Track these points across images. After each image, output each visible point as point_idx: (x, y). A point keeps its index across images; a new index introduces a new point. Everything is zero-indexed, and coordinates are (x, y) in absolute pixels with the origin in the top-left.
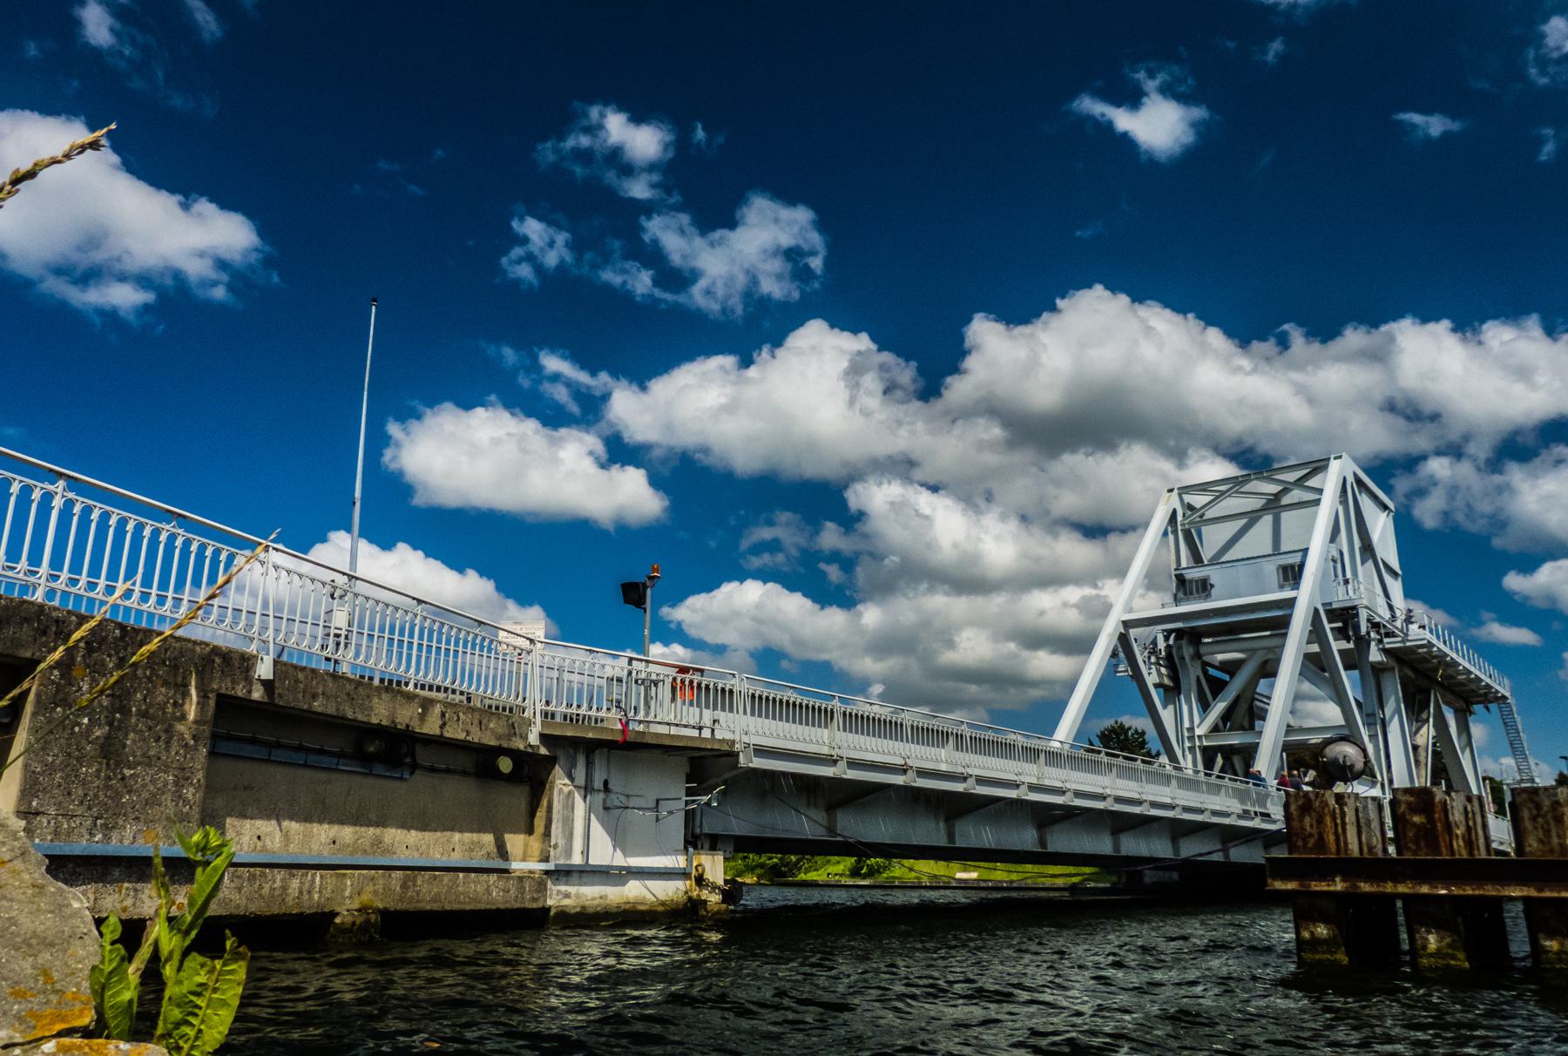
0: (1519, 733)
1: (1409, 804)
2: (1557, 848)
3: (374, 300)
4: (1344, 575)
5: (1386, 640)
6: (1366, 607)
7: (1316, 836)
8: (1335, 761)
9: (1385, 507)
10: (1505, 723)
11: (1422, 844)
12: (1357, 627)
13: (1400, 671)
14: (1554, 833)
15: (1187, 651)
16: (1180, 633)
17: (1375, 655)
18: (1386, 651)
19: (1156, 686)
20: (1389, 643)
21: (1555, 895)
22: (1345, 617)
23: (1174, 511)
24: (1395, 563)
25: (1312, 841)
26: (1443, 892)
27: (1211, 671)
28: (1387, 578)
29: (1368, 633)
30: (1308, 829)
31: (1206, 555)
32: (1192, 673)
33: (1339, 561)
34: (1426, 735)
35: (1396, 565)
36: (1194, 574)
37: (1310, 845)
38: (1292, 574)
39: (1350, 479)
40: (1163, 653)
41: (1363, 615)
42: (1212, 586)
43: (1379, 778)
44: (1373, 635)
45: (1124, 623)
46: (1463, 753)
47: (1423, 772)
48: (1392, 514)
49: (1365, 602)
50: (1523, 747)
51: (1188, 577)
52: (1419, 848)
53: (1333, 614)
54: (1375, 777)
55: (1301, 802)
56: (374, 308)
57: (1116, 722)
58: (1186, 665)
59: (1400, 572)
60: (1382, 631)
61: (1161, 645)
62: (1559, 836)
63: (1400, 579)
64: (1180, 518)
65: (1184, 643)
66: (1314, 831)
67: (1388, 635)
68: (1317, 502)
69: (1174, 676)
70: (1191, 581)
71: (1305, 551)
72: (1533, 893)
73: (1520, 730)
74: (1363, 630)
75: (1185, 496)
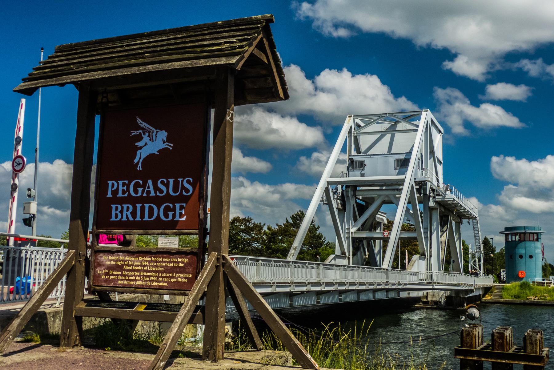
0: (478, 232)
1: (498, 336)
2: (534, 351)
3: (42, 49)
4: (422, 167)
5: (437, 197)
6: (430, 182)
7: (470, 343)
8: (471, 314)
9: (440, 132)
10: (474, 228)
11: (500, 348)
12: (425, 190)
13: (440, 209)
14: (534, 348)
15: (350, 193)
16: (347, 187)
17: (431, 204)
18: (436, 202)
19: (336, 208)
20: (438, 199)
21: (533, 364)
22: (421, 185)
23: (351, 127)
24: (441, 159)
25: (469, 344)
26: (504, 361)
27: (358, 201)
28: (438, 165)
29: (430, 193)
30: (468, 341)
31: (363, 148)
32: (351, 204)
33: (421, 159)
34: (444, 238)
35: (441, 159)
36: (358, 159)
37: (468, 345)
38: (403, 164)
39: (430, 122)
40: (340, 194)
41: (429, 185)
42: (365, 165)
43: (427, 256)
44: (431, 194)
45: (328, 182)
46: (457, 241)
47: (443, 252)
48: (442, 134)
49: (430, 179)
50: (479, 238)
51: (355, 160)
52: (499, 348)
53: (417, 183)
54: (425, 256)
55: (467, 333)
56: (42, 53)
57: (300, 211)
58: (349, 200)
59: (442, 161)
60: (436, 193)
61: (340, 190)
62: (536, 348)
63: (442, 164)
64: (353, 130)
65: (350, 189)
66: (470, 342)
67: (438, 195)
68: (416, 131)
69: (344, 205)
70: (356, 162)
71: (410, 153)
72: (527, 363)
73: (479, 231)
74: (428, 192)
75: (355, 120)
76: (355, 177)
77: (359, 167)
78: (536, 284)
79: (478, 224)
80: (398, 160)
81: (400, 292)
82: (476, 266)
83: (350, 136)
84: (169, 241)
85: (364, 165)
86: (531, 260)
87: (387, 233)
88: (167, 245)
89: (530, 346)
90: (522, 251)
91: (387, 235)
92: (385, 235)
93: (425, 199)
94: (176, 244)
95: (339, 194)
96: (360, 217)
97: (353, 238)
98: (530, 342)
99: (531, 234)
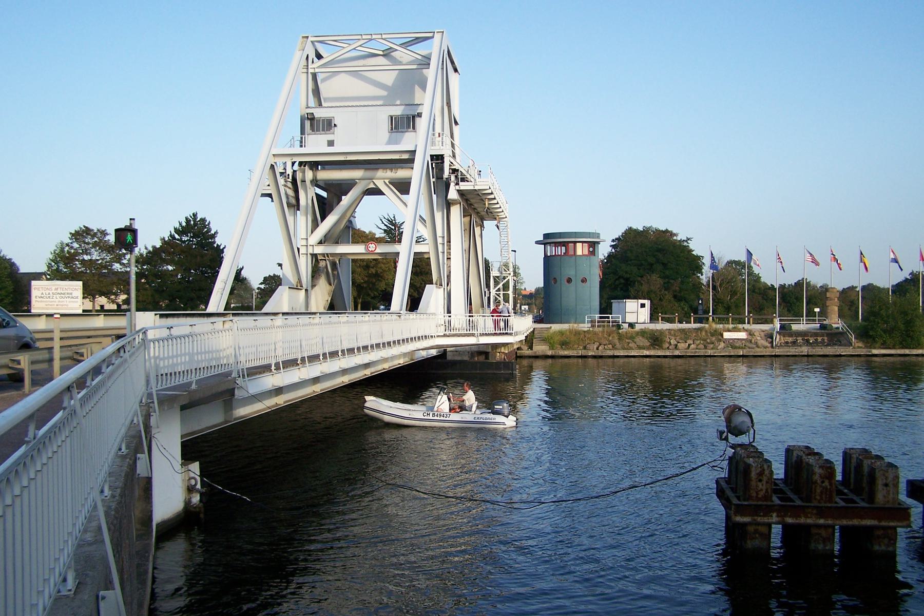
5: (461, 183)
7: (764, 491)
17: (453, 194)
20: (464, 186)
32: (307, 196)
36: (319, 113)
37: (760, 496)
51: (316, 116)
76: (317, 145)
77: (323, 130)
82: (500, 297)
84: (59, 291)
86: (583, 284)
89: (883, 489)
90: (571, 273)
91: (373, 250)
92: (370, 249)
94: (77, 297)
95: (288, 178)
96: (322, 221)
98: (884, 481)
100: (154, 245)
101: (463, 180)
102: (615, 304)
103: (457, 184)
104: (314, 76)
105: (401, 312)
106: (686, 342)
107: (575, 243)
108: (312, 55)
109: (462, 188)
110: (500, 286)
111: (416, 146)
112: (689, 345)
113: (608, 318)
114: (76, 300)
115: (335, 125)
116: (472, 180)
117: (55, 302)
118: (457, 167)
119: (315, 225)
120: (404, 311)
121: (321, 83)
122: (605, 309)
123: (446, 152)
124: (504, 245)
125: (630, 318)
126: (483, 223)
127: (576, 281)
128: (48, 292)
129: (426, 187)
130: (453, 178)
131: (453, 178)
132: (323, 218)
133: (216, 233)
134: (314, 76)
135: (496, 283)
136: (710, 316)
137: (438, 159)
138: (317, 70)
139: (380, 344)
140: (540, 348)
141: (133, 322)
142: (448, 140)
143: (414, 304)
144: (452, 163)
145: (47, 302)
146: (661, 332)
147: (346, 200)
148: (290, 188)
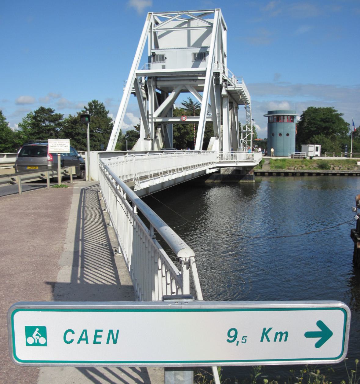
5: (228, 87)
17: (224, 92)
20: (229, 88)
29: (222, 83)
36: (157, 52)
51: (156, 53)
54: (218, 137)
65: (152, 80)
70: (158, 55)
74: (221, 82)
76: (156, 68)
77: (160, 60)
78: (294, 157)
79: (250, 109)
80: (195, 54)
81: (69, 139)
83: (151, 32)
84: (60, 143)
85: (165, 58)
87: (185, 117)
88: (58, 147)
90: (281, 130)
93: (219, 87)
94: (67, 146)
95: (143, 85)
97: (155, 123)
99: (288, 117)
100: (71, 114)
101: (229, 85)
102: (303, 146)
103: (226, 87)
104: (155, 33)
105: (200, 151)
106: (338, 166)
107: (284, 116)
108: (153, 23)
109: (228, 89)
110: (246, 137)
111: (206, 68)
112: (340, 168)
113: (300, 154)
114: (67, 147)
115: (166, 58)
116: (233, 85)
117: (58, 148)
118: (226, 78)
119: (156, 108)
120: (201, 150)
121: (159, 38)
122: (298, 149)
123: (221, 71)
124: (248, 118)
125: (310, 154)
126: (238, 106)
127: (284, 135)
128: (55, 144)
129: (210, 99)
130: (224, 84)
131: (224, 84)
132: (160, 104)
133: (109, 111)
134: (155, 33)
135: (244, 136)
136: (351, 153)
137: (217, 74)
138: (156, 31)
139: (182, 168)
140: (265, 169)
141: (89, 157)
142: (221, 65)
143: (205, 147)
144: (223, 76)
145: (55, 148)
146: (328, 161)
147: (171, 96)
148: (143, 90)
